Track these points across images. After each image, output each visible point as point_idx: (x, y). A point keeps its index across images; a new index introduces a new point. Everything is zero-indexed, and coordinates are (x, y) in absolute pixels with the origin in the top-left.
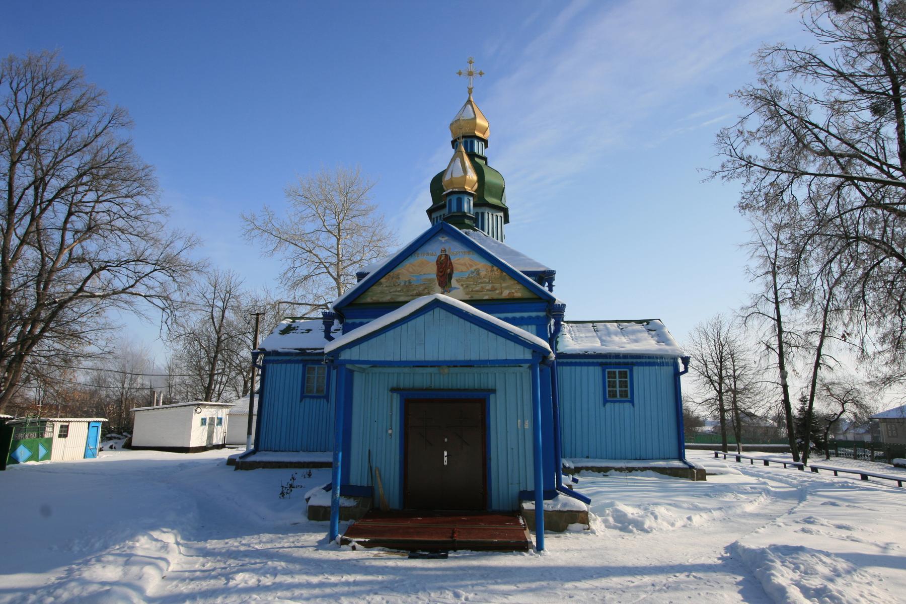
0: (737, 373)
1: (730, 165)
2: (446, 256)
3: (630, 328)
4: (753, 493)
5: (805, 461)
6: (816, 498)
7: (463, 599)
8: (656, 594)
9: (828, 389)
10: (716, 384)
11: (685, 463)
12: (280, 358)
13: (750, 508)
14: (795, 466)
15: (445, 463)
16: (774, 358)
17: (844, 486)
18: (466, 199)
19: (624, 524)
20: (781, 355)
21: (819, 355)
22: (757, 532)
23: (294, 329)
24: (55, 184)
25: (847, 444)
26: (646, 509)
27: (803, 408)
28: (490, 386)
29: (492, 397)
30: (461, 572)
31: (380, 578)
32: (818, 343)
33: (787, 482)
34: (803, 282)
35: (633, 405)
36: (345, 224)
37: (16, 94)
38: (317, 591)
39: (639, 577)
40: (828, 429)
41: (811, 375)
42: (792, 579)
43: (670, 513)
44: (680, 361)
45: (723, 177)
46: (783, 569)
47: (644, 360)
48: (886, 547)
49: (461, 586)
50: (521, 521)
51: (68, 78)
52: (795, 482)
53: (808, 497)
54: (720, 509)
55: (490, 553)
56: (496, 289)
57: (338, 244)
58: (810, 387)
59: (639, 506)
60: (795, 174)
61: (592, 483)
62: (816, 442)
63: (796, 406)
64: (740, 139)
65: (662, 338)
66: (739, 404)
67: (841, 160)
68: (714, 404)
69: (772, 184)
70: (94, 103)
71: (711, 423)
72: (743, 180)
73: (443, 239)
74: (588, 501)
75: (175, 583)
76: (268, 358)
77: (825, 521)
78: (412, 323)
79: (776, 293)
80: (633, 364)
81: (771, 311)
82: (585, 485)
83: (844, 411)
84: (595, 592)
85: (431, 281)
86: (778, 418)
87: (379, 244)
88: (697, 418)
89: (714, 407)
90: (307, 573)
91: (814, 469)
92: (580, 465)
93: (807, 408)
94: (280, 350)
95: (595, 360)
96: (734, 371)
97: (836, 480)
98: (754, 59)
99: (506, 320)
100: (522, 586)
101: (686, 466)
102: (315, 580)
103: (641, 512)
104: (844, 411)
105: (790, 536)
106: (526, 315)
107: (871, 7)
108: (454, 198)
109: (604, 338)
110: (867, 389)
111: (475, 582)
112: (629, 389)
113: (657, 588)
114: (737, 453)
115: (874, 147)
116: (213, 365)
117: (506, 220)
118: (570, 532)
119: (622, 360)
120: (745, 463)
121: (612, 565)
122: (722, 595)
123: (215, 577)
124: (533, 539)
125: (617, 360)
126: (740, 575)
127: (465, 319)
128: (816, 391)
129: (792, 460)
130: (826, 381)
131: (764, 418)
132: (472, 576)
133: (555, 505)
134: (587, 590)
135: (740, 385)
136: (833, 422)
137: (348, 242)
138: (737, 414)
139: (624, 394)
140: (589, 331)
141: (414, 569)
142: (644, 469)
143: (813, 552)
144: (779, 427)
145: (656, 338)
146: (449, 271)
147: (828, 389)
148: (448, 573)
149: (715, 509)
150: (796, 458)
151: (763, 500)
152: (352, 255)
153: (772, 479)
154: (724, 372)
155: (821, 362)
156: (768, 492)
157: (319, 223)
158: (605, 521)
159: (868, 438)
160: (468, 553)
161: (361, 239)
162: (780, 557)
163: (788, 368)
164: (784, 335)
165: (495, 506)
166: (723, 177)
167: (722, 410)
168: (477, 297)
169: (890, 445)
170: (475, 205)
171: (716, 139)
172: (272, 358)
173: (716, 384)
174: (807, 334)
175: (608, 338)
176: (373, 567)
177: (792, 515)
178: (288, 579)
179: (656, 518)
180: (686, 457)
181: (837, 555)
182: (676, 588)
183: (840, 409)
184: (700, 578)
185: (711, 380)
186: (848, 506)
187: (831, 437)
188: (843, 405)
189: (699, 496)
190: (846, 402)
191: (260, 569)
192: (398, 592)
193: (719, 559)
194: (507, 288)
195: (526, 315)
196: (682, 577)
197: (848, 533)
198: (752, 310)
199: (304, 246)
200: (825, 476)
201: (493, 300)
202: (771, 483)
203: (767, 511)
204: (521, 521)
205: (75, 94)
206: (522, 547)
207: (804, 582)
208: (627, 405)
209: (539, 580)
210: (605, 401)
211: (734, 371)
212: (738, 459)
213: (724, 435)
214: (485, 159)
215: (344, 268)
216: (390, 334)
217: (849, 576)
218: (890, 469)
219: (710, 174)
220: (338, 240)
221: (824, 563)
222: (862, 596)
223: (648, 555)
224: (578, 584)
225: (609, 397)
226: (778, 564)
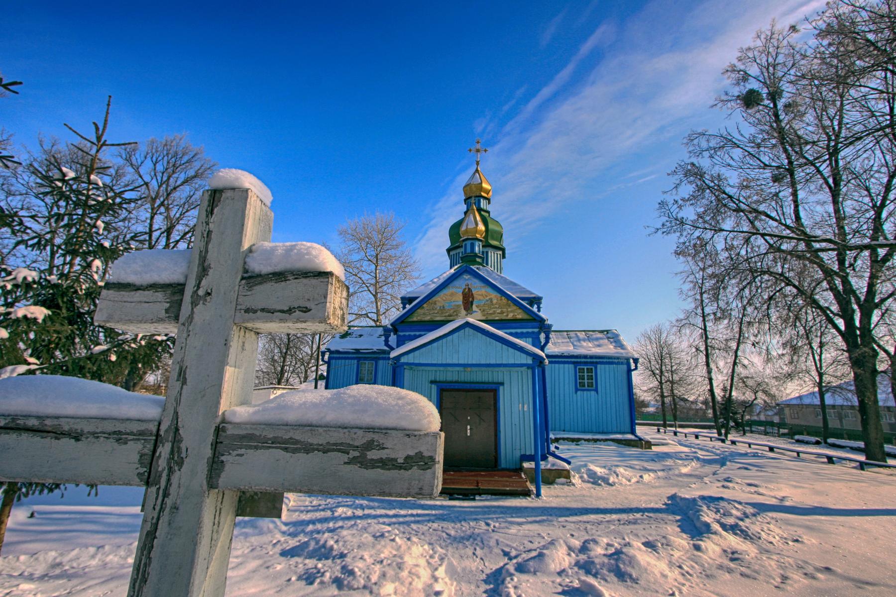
0: (674, 368)
1: (668, 224)
2: (469, 289)
3: (594, 336)
4: (687, 459)
5: (726, 436)
6: (733, 464)
7: (492, 526)
8: (621, 527)
9: (744, 382)
10: (658, 376)
11: (636, 436)
12: (341, 356)
13: (684, 470)
14: (719, 439)
15: (469, 434)
16: (702, 358)
17: (755, 455)
18: (477, 243)
19: (595, 479)
20: (707, 356)
21: (736, 356)
22: (690, 487)
23: (350, 334)
24: (180, 228)
25: (760, 423)
26: (610, 469)
27: (724, 396)
28: (500, 380)
29: (501, 388)
30: (486, 510)
31: (434, 512)
32: (735, 348)
33: (712, 452)
34: (722, 304)
35: (597, 393)
36: (382, 255)
37: (155, 165)
38: (394, 520)
39: (609, 515)
40: (744, 412)
41: (730, 371)
42: (714, 519)
43: (627, 473)
44: (631, 361)
45: (663, 233)
46: (708, 512)
47: (605, 360)
48: (783, 499)
49: (489, 519)
50: (523, 476)
51: (192, 154)
52: (718, 452)
53: (728, 463)
54: (663, 470)
55: (504, 497)
56: (504, 313)
57: (376, 270)
58: (729, 380)
59: (604, 467)
60: (715, 230)
61: (568, 450)
62: (735, 421)
63: (719, 393)
64: (676, 206)
65: (619, 344)
66: (675, 392)
67: (750, 216)
68: (656, 391)
69: (698, 238)
70: (209, 172)
71: (654, 406)
72: (678, 234)
73: (466, 277)
74: (569, 463)
75: (297, 514)
76: (332, 355)
77: (739, 481)
78: (450, 338)
79: (703, 310)
80: (597, 363)
81: (701, 325)
82: (564, 450)
83: (756, 399)
84: (580, 524)
85: (458, 306)
86: (705, 402)
87: (407, 270)
88: (643, 401)
89: (656, 394)
90: (384, 508)
91: (733, 443)
92: (558, 436)
93: (727, 395)
94: (341, 350)
95: (569, 360)
96: (672, 367)
97: (749, 451)
98: (685, 141)
99: (511, 334)
100: (530, 519)
101: (636, 439)
102: (391, 512)
103: (607, 471)
104: (756, 399)
105: (714, 490)
106: (525, 331)
107: (772, 105)
108: (469, 243)
109: (575, 343)
110: (774, 382)
111: (497, 516)
112: (594, 381)
113: (622, 522)
114: (674, 429)
115: (775, 206)
116: (285, 358)
117: (504, 257)
118: (557, 484)
119: (589, 360)
120: (681, 437)
121: (589, 507)
122: (666, 528)
123: (323, 510)
124: (533, 488)
125: (585, 360)
126: (679, 515)
127: (486, 336)
128: (735, 383)
129: (716, 435)
130: (742, 376)
131: (695, 402)
132: (495, 513)
133: (547, 465)
134: (574, 522)
135: (676, 378)
136: (748, 406)
137: (383, 268)
138: (674, 399)
139: (589, 385)
140: (564, 338)
141: (455, 507)
142: (606, 440)
143: (729, 501)
144: (706, 409)
145: (614, 344)
146: (471, 299)
147: (744, 382)
148: (478, 510)
149: (659, 470)
150: (720, 434)
151: (694, 464)
152: (386, 278)
153: (701, 449)
154: (664, 367)
155: (737, 361)
156: (698, 459)
157: (362, 253)
158: (581, 477)
159: (776, 420)
160: (489, 497)
161: (393, 266)
162: (706, 504)
163: (712, 366)
164: (709, 341)
165: (503, 465)
166: (663, 233)
167: (662, 396)
168: (490, 318)
169: (792, 425)
170: (483, 246)
171: (658, 206)
172: (335, 355)
173: (658, 376)
174: (727, 340)
175: (578, 344)
176: (426, 505)
177: (715, 476)
178: (372, 512)
179: (617, 475)
180: (637, 431)
181: (747, 504)
182: (635, 522)
183: (754, 398)
184: (651, 517)
185: (654, 374)
186: (757, 470)
187: (747, 417)
188: (755, 393)
189: (647, 461)
190: (757, 392)
191: (352, 505)
192: (448, 521)
193: (663, 504)
194: (511, 312)
195: (525, 331)
196: (638, 515)
197: (756, 489)
198: (684, 322)
199: (351, 271)
200: (742, 448)
201: (502, 320)
202: (700, 452)
203: (697, 473)
204: (523, 476)
205: (196, 165)
206: (526, 494)
207: (723, 520)
208: (593, 393)
209: (541, 516)
210: (577, 390)
211: (672, 367)
212: (675, 433)
213: (664, 415)
214: (488, 212)
215: (380, 287)
216: (435, 344)
217: (754, 518)
218: (793, 443)
219: (653, 230)
220: (376, 267)
221: (737, 508)
222: (762, 530)
223: (614, 501)
224: (567, 519)
225: (580, 386)
226: (705, 508)
